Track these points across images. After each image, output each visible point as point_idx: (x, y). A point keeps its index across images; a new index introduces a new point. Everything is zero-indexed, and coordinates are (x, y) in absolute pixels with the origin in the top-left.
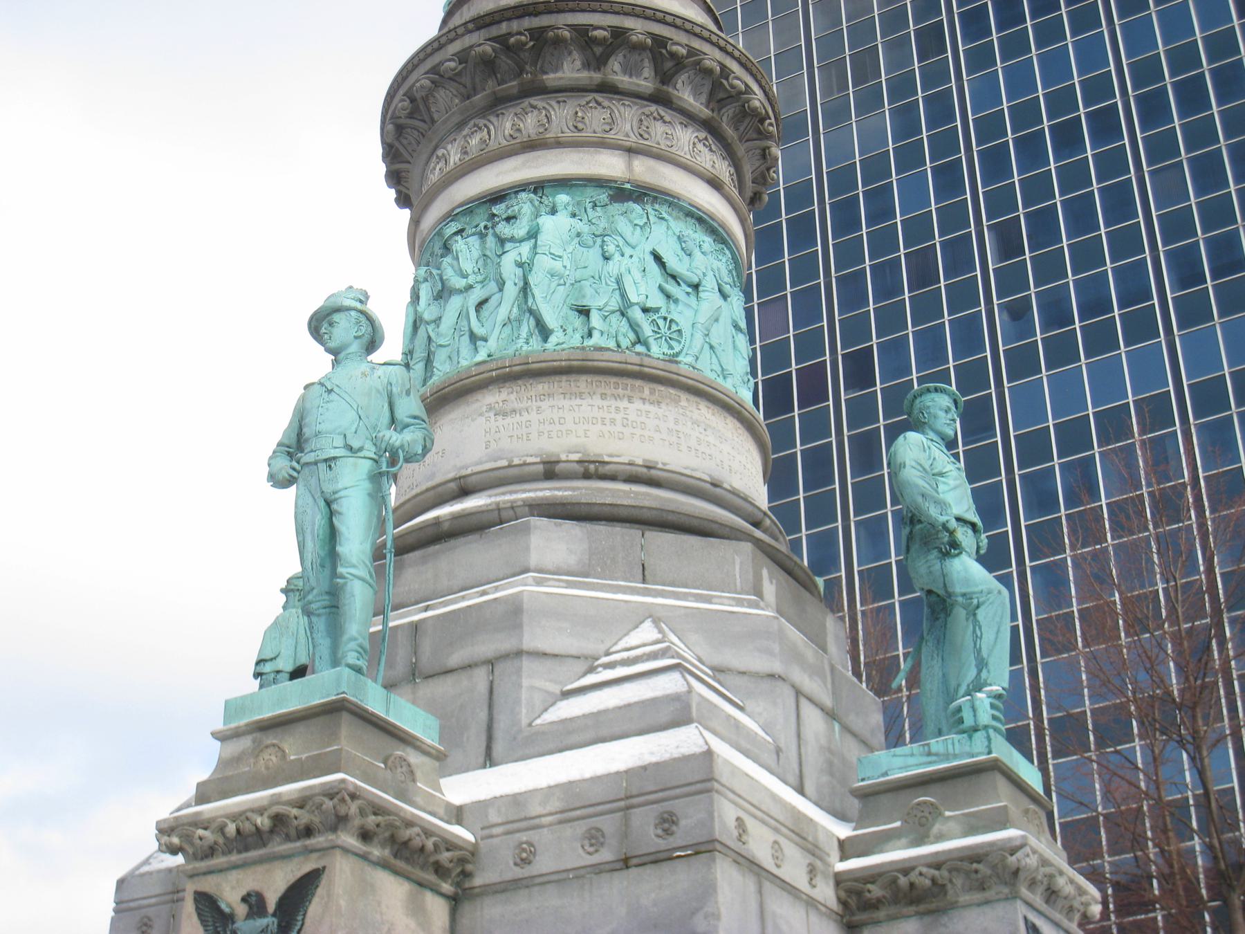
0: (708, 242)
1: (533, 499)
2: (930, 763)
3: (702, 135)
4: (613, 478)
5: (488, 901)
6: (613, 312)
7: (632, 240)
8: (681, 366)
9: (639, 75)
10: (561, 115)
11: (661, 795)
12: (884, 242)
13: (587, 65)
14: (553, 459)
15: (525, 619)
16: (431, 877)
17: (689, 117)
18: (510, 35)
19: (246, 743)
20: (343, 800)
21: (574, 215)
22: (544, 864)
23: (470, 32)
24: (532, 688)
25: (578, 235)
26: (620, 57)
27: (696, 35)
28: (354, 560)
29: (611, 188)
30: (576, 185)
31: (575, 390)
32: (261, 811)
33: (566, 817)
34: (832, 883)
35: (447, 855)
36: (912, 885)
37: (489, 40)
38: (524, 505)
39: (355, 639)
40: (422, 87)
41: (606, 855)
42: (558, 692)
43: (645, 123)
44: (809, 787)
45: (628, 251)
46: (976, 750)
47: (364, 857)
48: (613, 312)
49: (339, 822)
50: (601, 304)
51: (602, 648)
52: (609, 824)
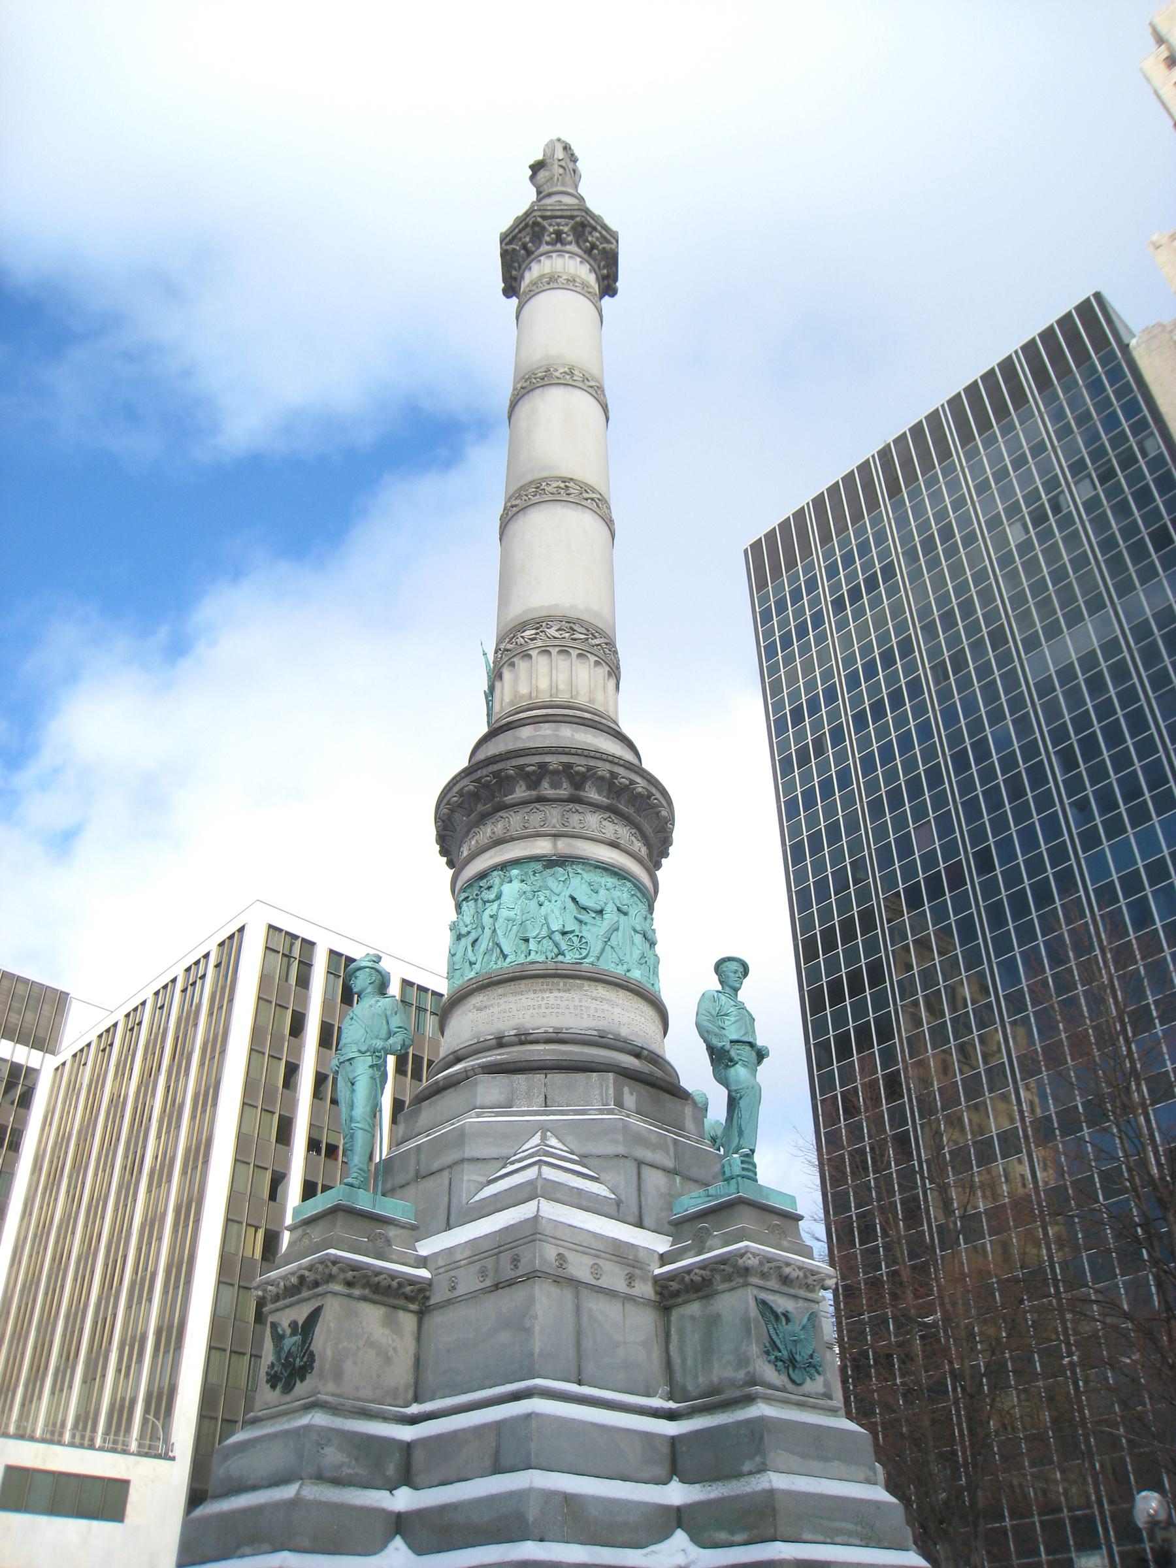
0: (609, 881)
3: (607, 815)
4: (537, 1042)
5: (436, 1313)
7: (557, 891)
10: (514, 821)
12: (987, 774)
13: (529, 788)
16: (402, 1302)
17: (596, 807)
18: (482, 777)
19: (300, 1232)
20: (327, 1266)
22: (461, 1290)
26: (547, 780)
32: (293, 1274)
33: (472, 1260)
34: (650, 1283)
35: (410, 1288)
41: (488, 1283)
44: (647, 1221)
45: (554, 898)
47: (349, 1296)
49: (330, 1278)
50: (534, 934)
51: (513, 1151)
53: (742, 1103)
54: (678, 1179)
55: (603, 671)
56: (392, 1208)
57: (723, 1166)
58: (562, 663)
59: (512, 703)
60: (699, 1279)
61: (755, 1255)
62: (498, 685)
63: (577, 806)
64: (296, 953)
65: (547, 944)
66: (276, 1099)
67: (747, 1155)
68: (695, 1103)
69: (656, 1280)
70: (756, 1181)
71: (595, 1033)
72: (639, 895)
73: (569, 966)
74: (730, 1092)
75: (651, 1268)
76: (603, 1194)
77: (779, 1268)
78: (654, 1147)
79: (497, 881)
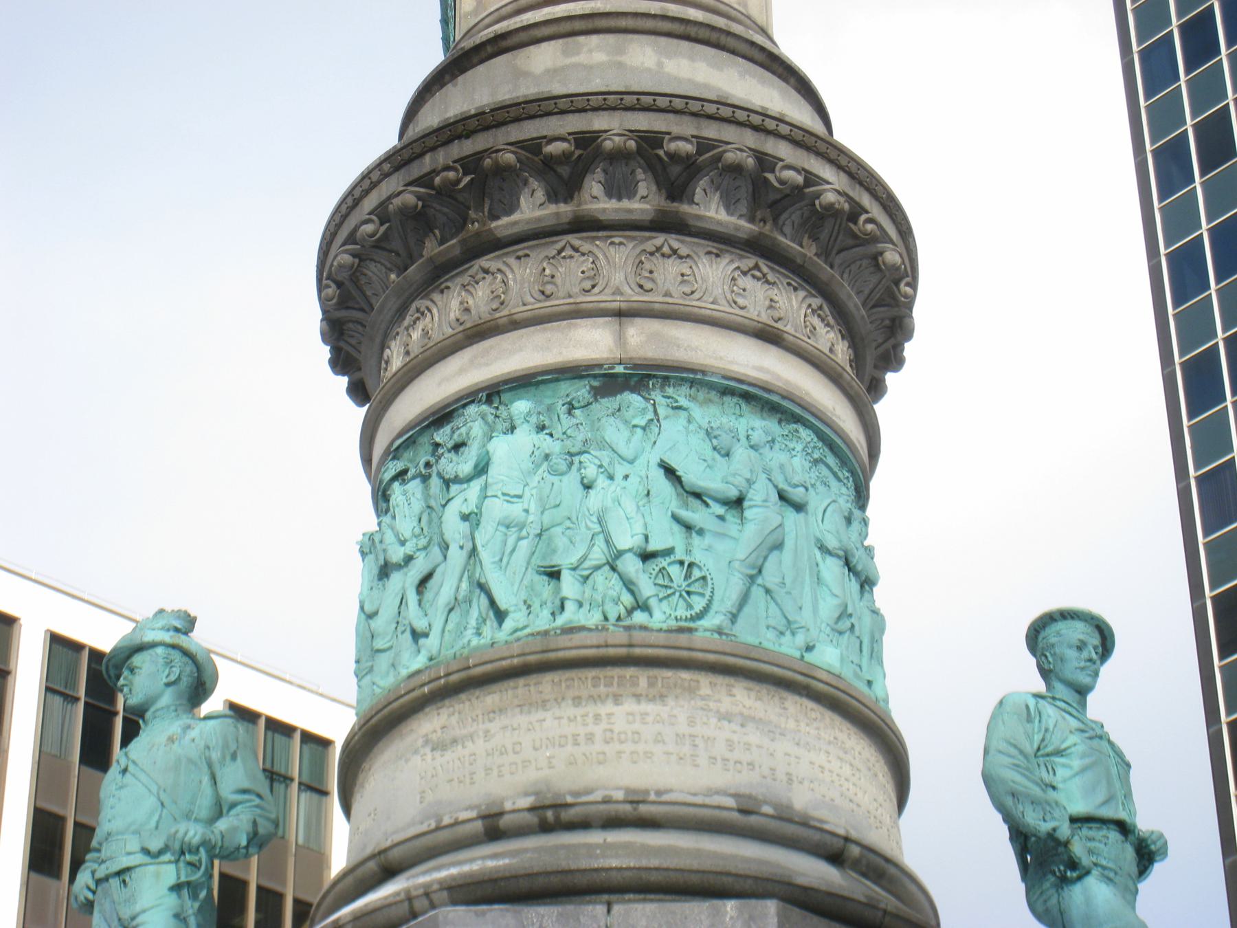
0: (758, 425)
1: (453, 878)
3: (750, 262)
4: (583, 825)
6: (597, 568)
8: (699, 634)
9: (631, 194)
10: (517, 279)
14: (495, 810)
17: (721, 241)
18: (435, 172)
21: (541, 428)
23: (387, 175)
25: (547, 457)
26: (599, 174)
27: (710, 117)
29: (595, 376)
30: (544, 382)
37: (407, 185)
38: (441, 889)
40: (341, 266)
43: (647, 266)
45: (620, 471)
48: (597, 568)
50: (574, 560)
63: (674, 241)
65: (607, 583)
71: (730, 802)
72: (831, 460)
73: (662, 638)
79: (477, 429)
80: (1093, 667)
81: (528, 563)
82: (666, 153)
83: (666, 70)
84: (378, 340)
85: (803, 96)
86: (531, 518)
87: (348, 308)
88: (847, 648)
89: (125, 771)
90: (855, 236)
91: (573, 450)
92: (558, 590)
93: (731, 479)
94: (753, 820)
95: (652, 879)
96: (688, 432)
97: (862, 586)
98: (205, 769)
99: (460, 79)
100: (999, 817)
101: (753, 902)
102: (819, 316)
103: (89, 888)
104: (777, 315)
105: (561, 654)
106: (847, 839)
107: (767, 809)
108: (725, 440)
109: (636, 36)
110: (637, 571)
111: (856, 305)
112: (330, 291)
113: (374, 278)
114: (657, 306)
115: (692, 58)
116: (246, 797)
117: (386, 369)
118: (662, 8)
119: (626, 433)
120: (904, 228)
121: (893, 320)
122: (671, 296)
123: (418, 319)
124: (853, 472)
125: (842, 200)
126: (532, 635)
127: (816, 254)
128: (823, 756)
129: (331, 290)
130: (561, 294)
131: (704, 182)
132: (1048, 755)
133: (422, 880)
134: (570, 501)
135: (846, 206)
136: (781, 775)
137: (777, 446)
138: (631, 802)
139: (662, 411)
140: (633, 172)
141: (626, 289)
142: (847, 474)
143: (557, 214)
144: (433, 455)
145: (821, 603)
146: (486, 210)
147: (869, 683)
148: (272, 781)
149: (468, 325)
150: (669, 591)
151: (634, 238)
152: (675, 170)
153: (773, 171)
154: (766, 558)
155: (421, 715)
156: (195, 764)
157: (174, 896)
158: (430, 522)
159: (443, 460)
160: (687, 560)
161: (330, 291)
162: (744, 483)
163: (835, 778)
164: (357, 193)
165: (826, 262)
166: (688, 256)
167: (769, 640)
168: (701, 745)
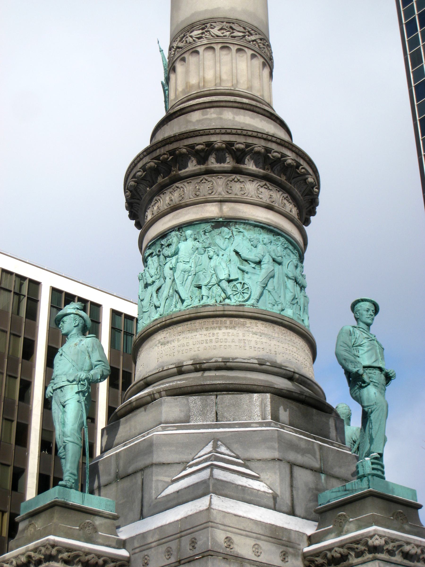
0: (266, 237)
1: (167, 387)
2: (346, 494)
3: (263, 183)
6: (214, 285)
7: (223, 247)
10: (187, 190)
11: (192, 530)
13: (199, 163)
15: (154, 448)
17: (254, 176)
18: (160, 155)
21: (195, 239)
23: (145, 156)
24: (157, 481)
25: (197, 249)
26: (214, 155)
27: (250, 136)
28: (69, 434)
29: (213, 222)
31: (194, 328)
32: (23, 554)
33: (160, 542)
34: (300, 559)
36: (333, 556)
39: (69, 471)
40: (131, 186)
42: (170, 481)
43: (230, 185)
44: (298, 510)
45: (221, 253)
46: (364, 487)
48: (214, 285)
50: (206, 283)
51: (191, 457)
52: (174, 545)
53: (373, 417)
54: (323, 476)
55: (258, 62)
56: (93, 502)
57: (357, 467)
58: (225, 57)
59: (184, 91)
60: (338, 555)
61: (381, 536)
62: (172, 76)
63: (238, 177)
64: (25, 291)
65: (216, 290)
66: (13, 410)
67: (376, 458)
68: (338, 416)
69: (305, 556)
70: (384, 478)
71: (256, 361)
72: (291, 247)
73: (234, 308)
74: (363, 407)
75: (301, 547)
76: (262, 489)
77: (401, 546)
78: (303, 452)
79: (175, 240)
80: (372, 317)
81: (191, 284)
82: (235, 148)
83: (236, 120)
84: (144, 209)
85: (281, 126)
86: (192, 269)
87: (134, 199)
88: (296, 309)
89: (61, 355)
90: (298, 173)
91: (206, 246)
92: (201, 293)
93: (257, 255)
94: (264, 367)
95: (231, 387)
96: (243, 240)
97: (301, 288)
98: (87, 354)
99: (169, 123)
100: (341, 367)
101: (263, 394)
102: (287, 200)
103: (51, 392)
104: (272, 200)
105: (202, 314)
106: (294, 372)
107: (268, 364)
108: (255, 243)
109: (226, 109)
110: (226, 286)
111: (299, 196)
112: (128, 194)
113: (142, 189)
114: (233, 199)
115: (244, 116)
116: (100, 363)
117: (146, 219)
118: (234, 99)
119: (223, 241)
120: (315, 170)
121: (312, 199)
122: (238, 195)
123: (156, 203)
124: (298, 251)
125: (293, 162)
126: (192, 307)
127: (285, 180)
128: (286, 345)
129: (128, 193)
130: (202, 195)
131: (248, 157)
132: (357, 346)
133: (157, 388)
134: (205, 263)
135: (295, 164)
136: (273, 352)
137: (272, 244)
138: (224, 362)
139: (235, 233)
140: (225, 154)
141: (223, 193)
142: (296, 252)
143: (200, 169)
144: (161, 248)
145: (287, 295)
146: (177, 167)
147: (303, 320)
148: (127, 335)
149: (172, 206)
150: (237, 292)
151: (225, 176)
152: (239, 153)
153: (270, 153)
154: (268, 281)
155: (157, 333)
156: (84, 352)
157: (77, 395)
158: (160, 270)
159: (164, 250)
160: (243, 282)
161: (128, 194)
162: (261, 256)
163: (291, 352)
164: (136, 162)
165: (289, 182)
166: (243, 182)
167: (269, 308)
168: (247, 343)
